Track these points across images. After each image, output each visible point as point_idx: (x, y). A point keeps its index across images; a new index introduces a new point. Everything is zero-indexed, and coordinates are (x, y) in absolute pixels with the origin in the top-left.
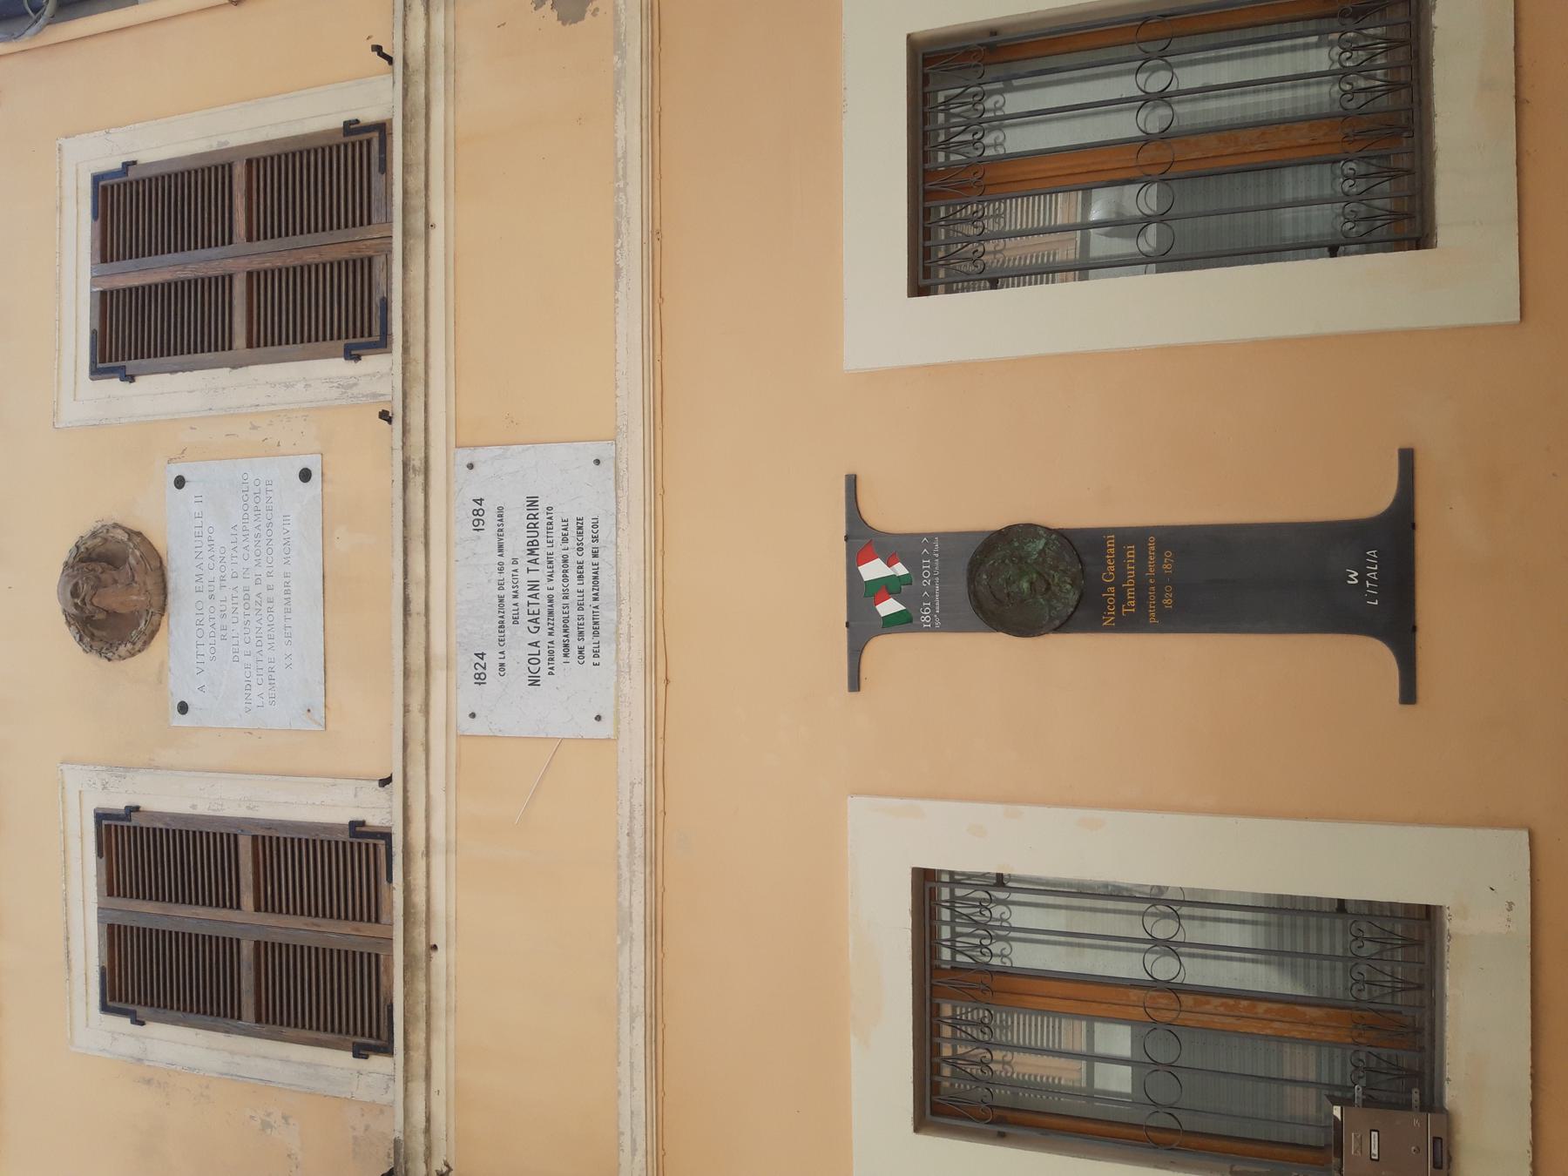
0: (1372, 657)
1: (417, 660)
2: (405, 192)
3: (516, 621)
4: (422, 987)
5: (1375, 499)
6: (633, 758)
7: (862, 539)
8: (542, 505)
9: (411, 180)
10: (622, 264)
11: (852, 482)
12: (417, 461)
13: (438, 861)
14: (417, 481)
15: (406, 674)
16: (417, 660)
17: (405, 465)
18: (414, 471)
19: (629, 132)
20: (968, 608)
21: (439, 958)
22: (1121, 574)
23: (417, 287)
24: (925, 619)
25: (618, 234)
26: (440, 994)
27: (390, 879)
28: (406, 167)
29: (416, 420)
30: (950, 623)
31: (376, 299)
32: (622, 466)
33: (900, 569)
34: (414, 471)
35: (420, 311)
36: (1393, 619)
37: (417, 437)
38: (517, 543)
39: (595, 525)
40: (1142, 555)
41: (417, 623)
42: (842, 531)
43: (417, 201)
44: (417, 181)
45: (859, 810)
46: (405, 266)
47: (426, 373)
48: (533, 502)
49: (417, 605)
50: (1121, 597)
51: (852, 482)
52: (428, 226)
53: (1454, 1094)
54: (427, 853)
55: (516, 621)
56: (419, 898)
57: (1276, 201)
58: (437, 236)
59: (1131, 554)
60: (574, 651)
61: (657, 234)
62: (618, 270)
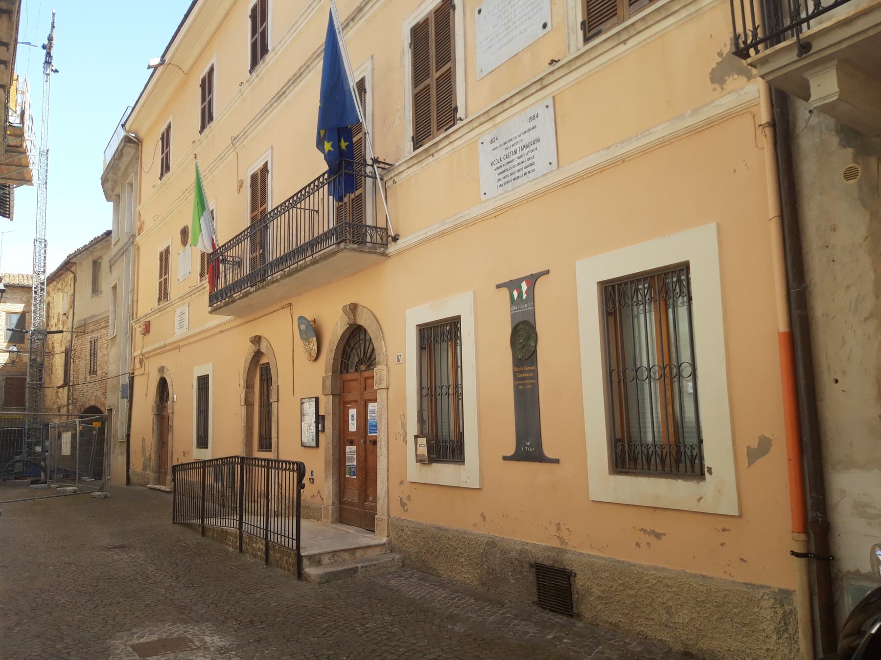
0: (511, 451)
1: (492, 114)
2: (633, 24)
3: (507, 149)
4: (424, 157)
5: (548, 453)
6: (476, 211)
7: (532, 280)
8: (537, 145)
9: (639, 23)
10: (611, 149)
11: (547, 272)
12: (545, 82)
13: (449, 148)
14: (538, 86)
15: (487, 112)
16: (492, 114)
17: (541, 79)
18: (541, 83)
19: (661, 131)
20: (516, 323)
21: (431, 159)
22: (526, 372)
23: (601, 50)
24: (514, 308)
25: (621, 143)
26: (424, 163)
27: (446, 130)
28: (643, 19)
29: (557, 75)
30: (513, 316)
31: (601, 27)
32: (549, 175)
33: (524, 296)
34: (541, 83)
35: (593, 56)
36: (521, 455)
37: (552, 78)
38: (527, 139)
39: (533, 171)
40: (530, 378)
41: (500, 109)
42: (534, 273)
43: (632, 31)
44: (640, 27)
45: (469, 295)
46: (605, 40)
47: (580, 67)
48: (538, 140)
49: (506, 105)
50: (521, 372)
51: (547, 272)
52: (624, 42)
53: (435, 466)
54: (450, 143)
55: (507, 149)
56: (440, 146)
57: (695, 430)
58: (622, 48)
59: (531, 375)
60: (531, 162)
61: (222, 332)
62: (608, 148)
